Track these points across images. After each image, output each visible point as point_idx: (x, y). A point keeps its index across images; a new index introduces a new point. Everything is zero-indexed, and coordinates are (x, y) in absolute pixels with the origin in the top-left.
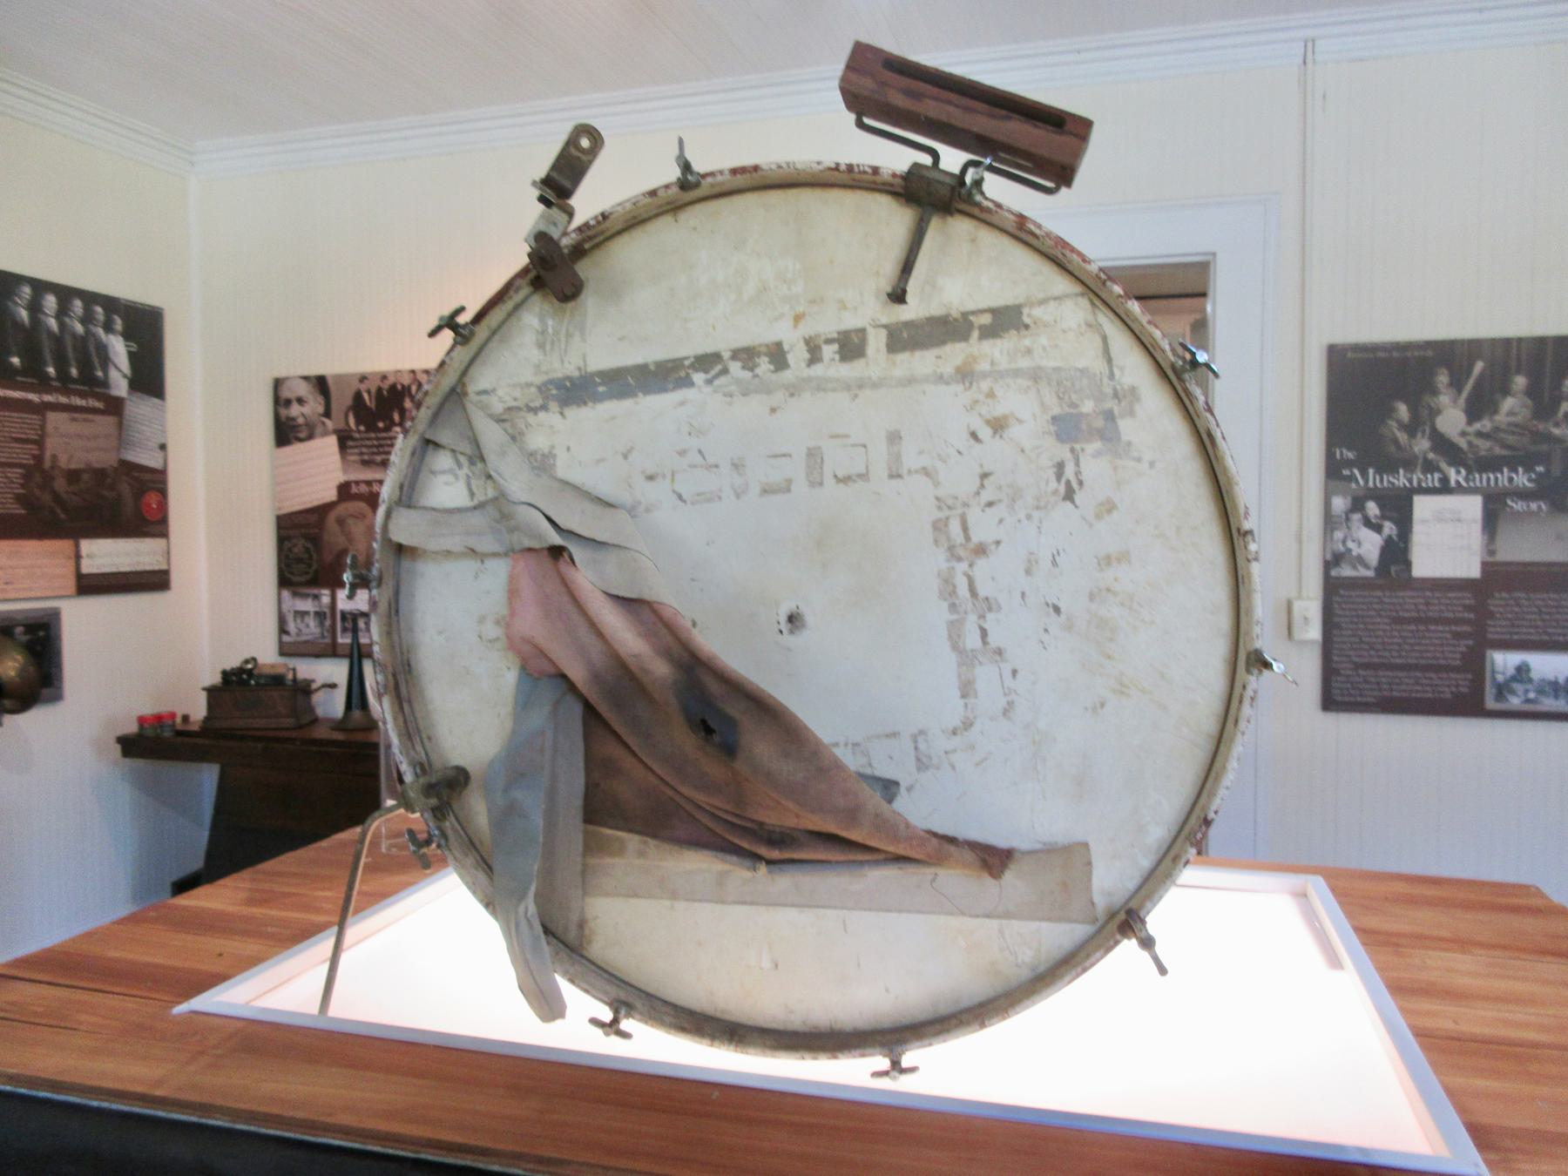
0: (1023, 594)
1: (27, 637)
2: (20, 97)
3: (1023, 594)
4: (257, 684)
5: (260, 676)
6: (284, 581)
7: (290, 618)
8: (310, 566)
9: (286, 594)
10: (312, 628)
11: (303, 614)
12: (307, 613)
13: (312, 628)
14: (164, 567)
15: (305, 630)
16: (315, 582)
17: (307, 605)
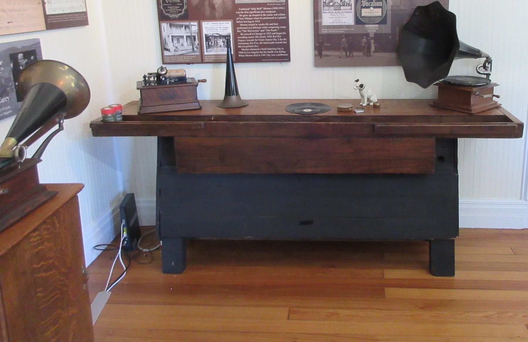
0: (9, 23)
1: (26, 61)
3: (9, 23)
4: (170, 83)
5: (170, 78)
6: (162, 17)
7: (169, 40)
8: (182, 7)
9: (165, 25)
10: (185, 47)
11: (179, 38)
12: (182, 37)
13: (185, 47)
14: (85, 10)
15: (181, 48)
16: (185, 17)
17: (182, 32)
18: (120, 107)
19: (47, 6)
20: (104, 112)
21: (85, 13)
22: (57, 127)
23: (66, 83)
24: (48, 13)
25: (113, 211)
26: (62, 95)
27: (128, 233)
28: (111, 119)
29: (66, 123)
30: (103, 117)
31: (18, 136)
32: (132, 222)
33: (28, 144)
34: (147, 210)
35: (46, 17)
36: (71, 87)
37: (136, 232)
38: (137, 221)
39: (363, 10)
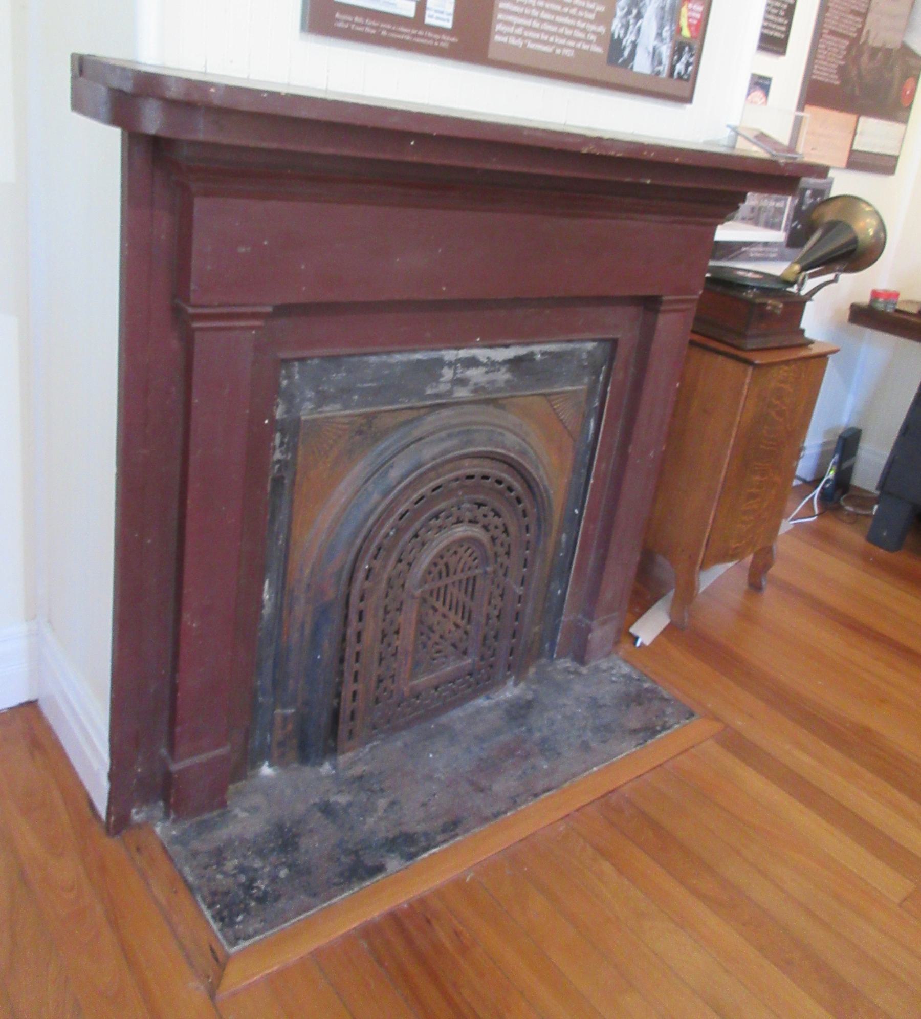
2: (535, 452)
18: (896, 295)
19: (857, 137)
20: (875, 295)
21: (896, 158)
22: (830, 277)
23: (865, 228)
24: (855, 147)
25: (824, 444)
26: (855, 241)
27: (837, 474)
28: (880, 305)
29: (844, 277)
30: (872, 301)
31: (804, 263)
32: (846, 465)
33: (812, 276)
34: (871, 463)
35: (852, 152)
36: (868, 234)
37: (843, 483)
38: (850, 470)
39: (428, 20)
